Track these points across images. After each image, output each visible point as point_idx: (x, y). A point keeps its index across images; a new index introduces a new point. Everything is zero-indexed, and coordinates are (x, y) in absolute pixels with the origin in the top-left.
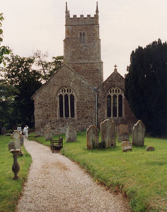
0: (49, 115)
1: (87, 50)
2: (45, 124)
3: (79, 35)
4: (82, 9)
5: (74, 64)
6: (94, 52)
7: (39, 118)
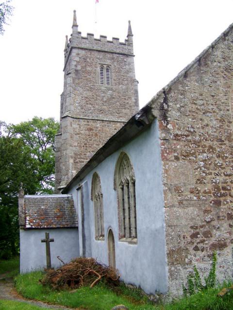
0: (224, 188)
1: (114, 98)
2: (207, 228)
3: (99, 69)
4: (105, 26)
5: (88, 122)
6: (128, 103)
7: (181, 203)
